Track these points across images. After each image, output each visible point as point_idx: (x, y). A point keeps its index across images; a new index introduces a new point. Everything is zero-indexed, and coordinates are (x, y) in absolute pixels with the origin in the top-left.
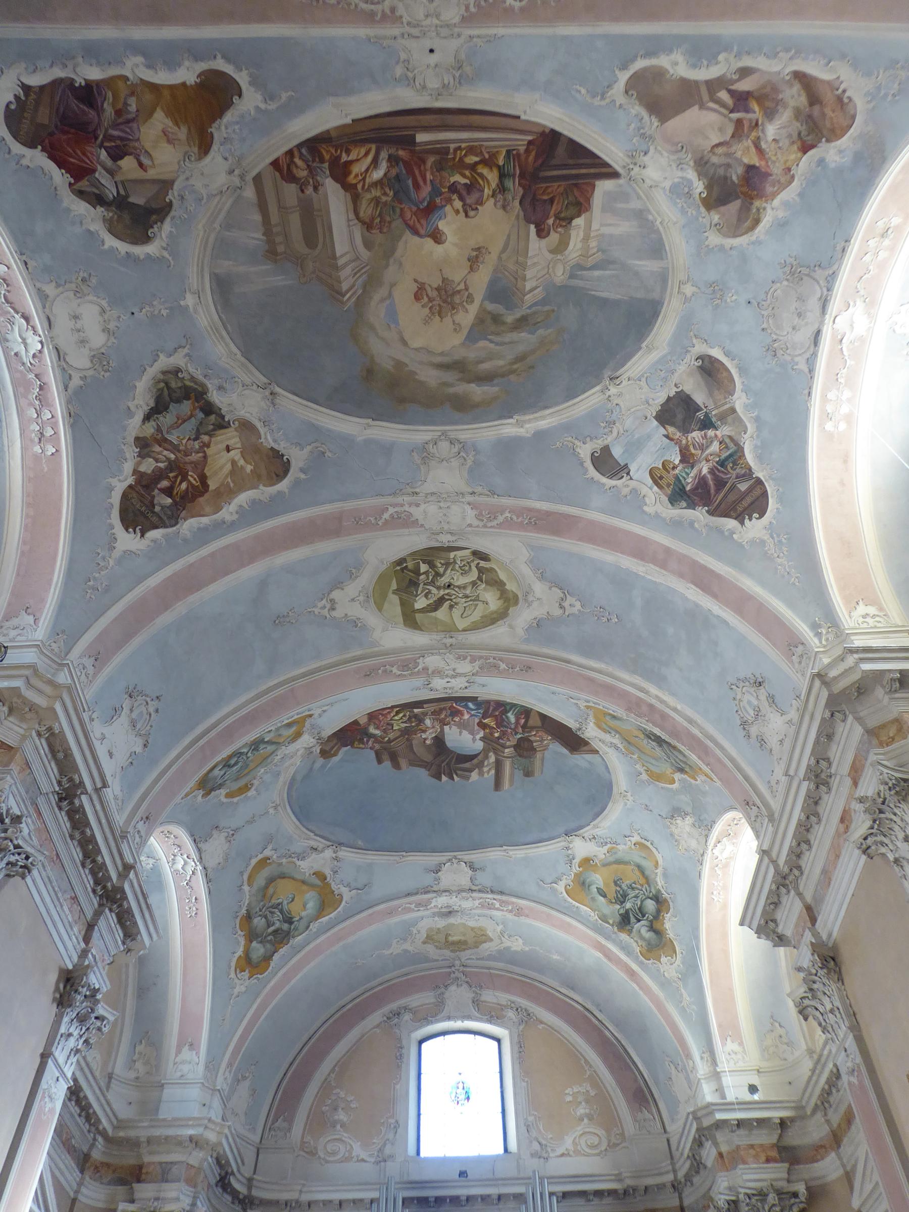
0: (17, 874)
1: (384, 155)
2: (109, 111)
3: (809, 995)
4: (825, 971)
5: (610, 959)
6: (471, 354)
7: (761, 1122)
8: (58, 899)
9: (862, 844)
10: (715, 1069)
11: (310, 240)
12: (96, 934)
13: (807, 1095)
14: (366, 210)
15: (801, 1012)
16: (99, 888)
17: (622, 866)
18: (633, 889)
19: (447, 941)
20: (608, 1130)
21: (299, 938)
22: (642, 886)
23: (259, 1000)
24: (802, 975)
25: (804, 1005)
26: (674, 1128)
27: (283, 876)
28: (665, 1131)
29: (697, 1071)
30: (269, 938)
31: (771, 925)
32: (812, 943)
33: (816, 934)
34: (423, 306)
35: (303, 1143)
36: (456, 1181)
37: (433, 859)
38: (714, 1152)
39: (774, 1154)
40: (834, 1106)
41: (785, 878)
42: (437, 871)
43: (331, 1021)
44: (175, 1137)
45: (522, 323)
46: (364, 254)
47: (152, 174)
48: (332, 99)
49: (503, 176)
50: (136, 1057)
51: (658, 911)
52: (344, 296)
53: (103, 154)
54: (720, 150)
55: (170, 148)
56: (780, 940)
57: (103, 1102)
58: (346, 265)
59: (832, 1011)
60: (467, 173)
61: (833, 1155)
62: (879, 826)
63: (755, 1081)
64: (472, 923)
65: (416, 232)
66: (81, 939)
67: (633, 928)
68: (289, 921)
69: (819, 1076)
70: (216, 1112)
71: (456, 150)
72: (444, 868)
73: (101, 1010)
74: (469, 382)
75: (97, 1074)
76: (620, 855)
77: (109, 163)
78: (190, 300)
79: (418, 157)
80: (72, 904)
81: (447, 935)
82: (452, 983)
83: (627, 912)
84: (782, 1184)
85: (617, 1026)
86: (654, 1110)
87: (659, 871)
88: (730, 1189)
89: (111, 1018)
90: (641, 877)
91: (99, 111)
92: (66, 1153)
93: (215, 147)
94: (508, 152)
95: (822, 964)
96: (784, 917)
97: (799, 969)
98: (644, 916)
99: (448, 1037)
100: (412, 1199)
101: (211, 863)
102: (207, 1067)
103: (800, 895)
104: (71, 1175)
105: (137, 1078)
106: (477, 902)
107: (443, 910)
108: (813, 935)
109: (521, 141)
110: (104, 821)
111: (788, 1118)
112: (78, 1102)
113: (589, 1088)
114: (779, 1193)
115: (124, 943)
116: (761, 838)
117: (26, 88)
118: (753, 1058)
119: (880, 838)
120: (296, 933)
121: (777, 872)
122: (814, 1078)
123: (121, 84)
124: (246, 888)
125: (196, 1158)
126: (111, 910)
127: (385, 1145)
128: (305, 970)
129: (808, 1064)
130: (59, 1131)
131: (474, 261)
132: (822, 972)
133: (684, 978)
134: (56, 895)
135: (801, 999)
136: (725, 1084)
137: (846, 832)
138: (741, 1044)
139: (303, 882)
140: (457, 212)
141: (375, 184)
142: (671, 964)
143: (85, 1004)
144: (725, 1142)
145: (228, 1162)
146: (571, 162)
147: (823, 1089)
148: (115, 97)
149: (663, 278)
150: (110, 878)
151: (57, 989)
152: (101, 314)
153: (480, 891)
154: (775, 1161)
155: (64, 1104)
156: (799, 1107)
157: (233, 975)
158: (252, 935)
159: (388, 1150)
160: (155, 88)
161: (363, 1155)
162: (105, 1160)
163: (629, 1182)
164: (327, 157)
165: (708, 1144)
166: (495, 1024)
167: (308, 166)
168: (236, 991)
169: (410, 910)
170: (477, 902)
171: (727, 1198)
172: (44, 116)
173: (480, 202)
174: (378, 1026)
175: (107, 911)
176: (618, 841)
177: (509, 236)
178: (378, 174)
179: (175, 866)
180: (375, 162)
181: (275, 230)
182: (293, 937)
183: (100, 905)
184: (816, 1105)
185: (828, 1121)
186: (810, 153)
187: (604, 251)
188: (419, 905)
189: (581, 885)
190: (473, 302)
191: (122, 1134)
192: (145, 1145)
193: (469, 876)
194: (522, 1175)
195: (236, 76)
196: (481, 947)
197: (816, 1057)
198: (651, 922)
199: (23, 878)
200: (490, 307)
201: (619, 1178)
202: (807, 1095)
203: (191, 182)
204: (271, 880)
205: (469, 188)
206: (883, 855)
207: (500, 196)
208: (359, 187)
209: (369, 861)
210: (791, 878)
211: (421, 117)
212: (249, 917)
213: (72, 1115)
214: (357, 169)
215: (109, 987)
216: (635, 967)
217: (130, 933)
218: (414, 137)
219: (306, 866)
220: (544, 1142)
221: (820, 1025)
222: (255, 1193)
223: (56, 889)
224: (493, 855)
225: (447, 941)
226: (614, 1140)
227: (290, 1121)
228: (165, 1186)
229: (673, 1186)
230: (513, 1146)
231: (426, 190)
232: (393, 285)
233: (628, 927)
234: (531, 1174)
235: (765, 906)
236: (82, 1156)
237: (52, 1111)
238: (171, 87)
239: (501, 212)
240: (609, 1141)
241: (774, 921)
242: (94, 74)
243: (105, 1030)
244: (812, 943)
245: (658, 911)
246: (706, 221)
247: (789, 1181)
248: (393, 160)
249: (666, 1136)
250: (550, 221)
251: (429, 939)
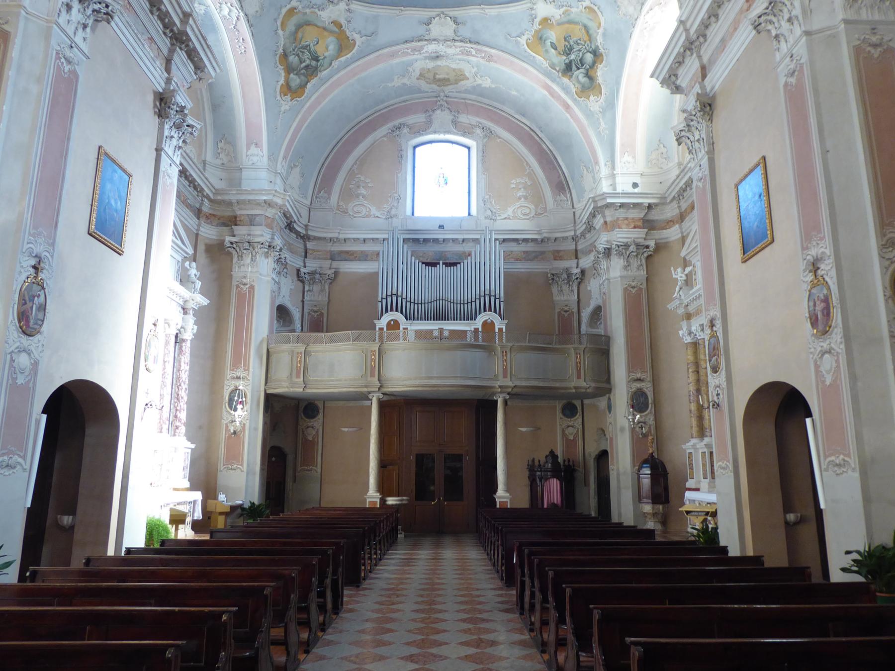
0: (103, 19)
3: (686, 129)
4: (702, 113)
5: (553, 96)
7: (636, 205)
9: (755, 21)
10: (613, 172)
12: (174, 67)
13: (668, 192)
15: (677, 140)
16: (168, 31)
17: (572, 26)
18: (578, 44)
19: (435, 78)
20: (536, 206)
21: (325, 72)
22: (585, 42)
23: (300, 116)
24: (685, 115)
25: (681, 135)
26: (579, 206)
27: (308, 23)
28: (573, 208)
29: (601, 173)
30: (302, 72)
31: (673, 78)
32: (698, 94)
33: (703, 87)
35: (338, 206)
36: (437, 230)
37: (425, 13)
38: (602, 221)
39: (640, 223)
40: (686, 198)
41: (692, 43)
42: (428, 24)
43: (352, 131)
44: (255, 200)
50: (219, 151)
51: (594, 63)
56: (677, 89)
57: (203, 178)
59: (698, 140)
61: (677, 226)
62: (772, 7)
63: (638, 180)
64: (454, 66)
66: (164, 71)
67: (573, 74)
68: (316, 59)
69: (681, 180)
70: (279, 186)
72: (434, 22)
73: (190, 120)
75: (195, 161)
76: (572, 16)
80: (151, 44)
81: (435, 74)
82: (438, 109)
83: (571, 62)
84: (641, 241)
85: (551, 142)
86: (568, 195)
87: (601, 31)
88: (607, 241)
89: (198, 127)
90: (586, 35)
92: (185, 207)
95: (701, 109)
96: (684, 73)
97: (684, 111)
98: (582, 65)
99: (433, 144)
100: (409, 239)
101: (251, 11)
102: (269, 159)
103: (700, 57)
104: (193, 221)
105: (223, 164)
106: (458, 50)
107: (433, 55)
108: (701, 87)
111: (654, 203)
112: (186, 178)
113: (527, 180)
114: (638, 245)
115: (196, 74)
116: (683, 10)
118: (641, 165)
119: (771, 17)
120: (322, 68)
121: (687, 38)
122: (678, 181)
124: (280, 32)
125: (270, 212)
126: (181, 49)
127: (392, 208)
128: (332, 95)
129: (676, 172)
130: (178, 196)
132: (699, 114)
133: (603, 112)
134: (137, 36)
135: (680, 131)
136: (617, 181)
137: (747, 10)
138: (634, 157)
139: (325, 29)
142: (597, 102)
143: (177, 116)
144: (610, 215)
145: (291, 215)
147: (682, 187)
150: (175, 24)
151: (155, 106)
153: (461, 41)
154: (639, 227)
155: (178, 179)
156: (663, 198)
157: (279, 98)
158: (289, 69)
159: (393, 212)
161: (378, 214)
162: (212, 212)
163: (546, 235)
165: (599, 217)
166: (467, 137)
168: (283, 109)
169: (407, 54)
170: (458, 50)
171: (605, 246)
174: (384, 136)
175: (178, 49)
176: (573, 5)
179: (222, 13)
182: (320, 72)
183: (172, 44)
184: (674, 197)
185: (679, 207)
188: (414, 50)
189: (540, 38)
191: (219, 197)
192: (236, 204)
193: (453, 28)
194: (479, 229)
196: (460, 84)
197: (682, 167)
198: (587, 70)
199: (109, 23)
201: (539, 232)
202: (670, 190)
204: (299, 27)
206: (769, 31)
209: (374, 13)
210: (697, 43)
212: (285, 55)
213: (184, 186)
215: (192, 105)
216: (570, 102)
217: (199, 67)
219: (327, 15)
220: (494, 211)
221: (688, 149)
222: (310, 233)
223: (136, 31)
224: (472, 12)
225: (435, 78)
226: (539, 211)
227: (329, 193)
228: (253, 227)
229: (573, 238)
230: (474, 212)
233: (570, 73)
234: (484, 228)
235: (671, 65)
236: (197, 211)
237: (172, 184)
240: (536, 212)
241: (676, 75)
243: (196, 134)
244: (698, 94)
245: (594, 63)
247: (645, 239)
249: (573, 210)
251: (422, 76)
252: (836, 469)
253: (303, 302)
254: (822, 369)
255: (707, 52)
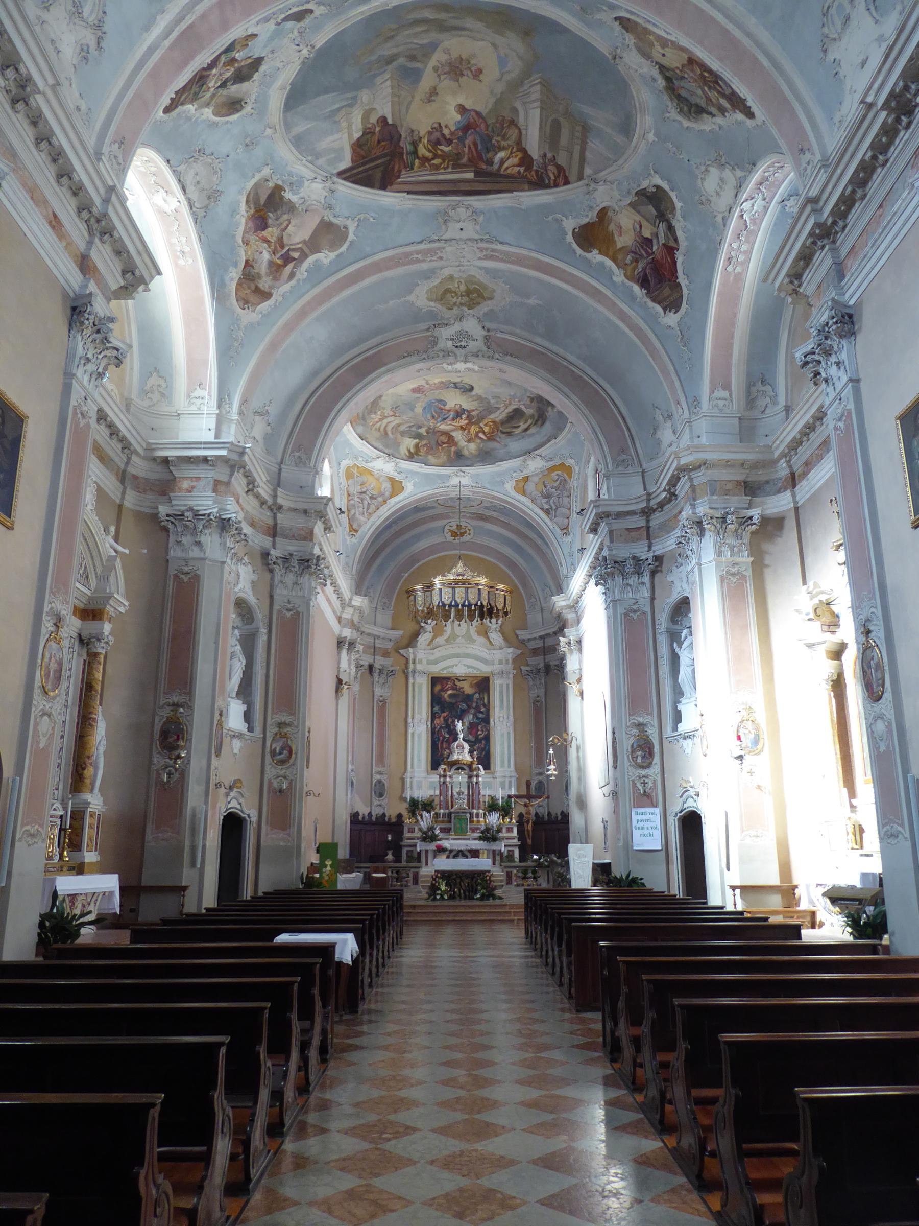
1: (496, 166)
2: (641, 266)
6: (433, 36)
8: (889, 222)
11: (556, 127)
14: (513, 133)
34: (475, 65)
45: (390, 60)
46: (518, 105)
47: (638, 218)
48: (523, 207)
49: (415, 152)
52: (540, 83)
53: (655, 248)
54: (285, 224)
55: (622, 224)
58: (534, 101)
60: (439, 152)
65: (478, 114)
71: (447, 167)
74: (436, 20)
75: (118, 401)
77: (655, 241)
78: (651, 137)
79: (473, 163)
91: (644, 269)
93: (599, 209)
94: (412, 168)
109: (405, 177)
110: (839, 171)
117: (665, 309)
123: (629, 274)
131: (433, 93)
134: (885, 227)
140: (446, 126)
141: (504, 149)
146: (370, 172)
148: (634, 269)
149: (288, 126)
152: (705, 179)
160: (615, 260)
164: (533, 173)
167: (546, 171)
172: (667, 291)
173: (430, 133)
177: (407, 112)
178: (502, 154)
180: (502, 162)
181: (579, 142)
186: (243, 264)
187: (335, 122)
190: (434, 68)
195: (573, 241)
200: (418, 65)
203: (619, 197)
205: (438, 142)
207: (416, 138)
208: (515, 149)
211: (469, 188)
214: (515, 161)
218: (475, 176)
231: (469, 141)
232: (500, 79)
238: (607, 256)
239: (414, 128)
242: (636, 288)
246: (275, 178)
248: (490, 163)
250: (377, 129)
252: (29, 839)
253: (271, 597)
254: (39, 728)
255: (846, 241)
